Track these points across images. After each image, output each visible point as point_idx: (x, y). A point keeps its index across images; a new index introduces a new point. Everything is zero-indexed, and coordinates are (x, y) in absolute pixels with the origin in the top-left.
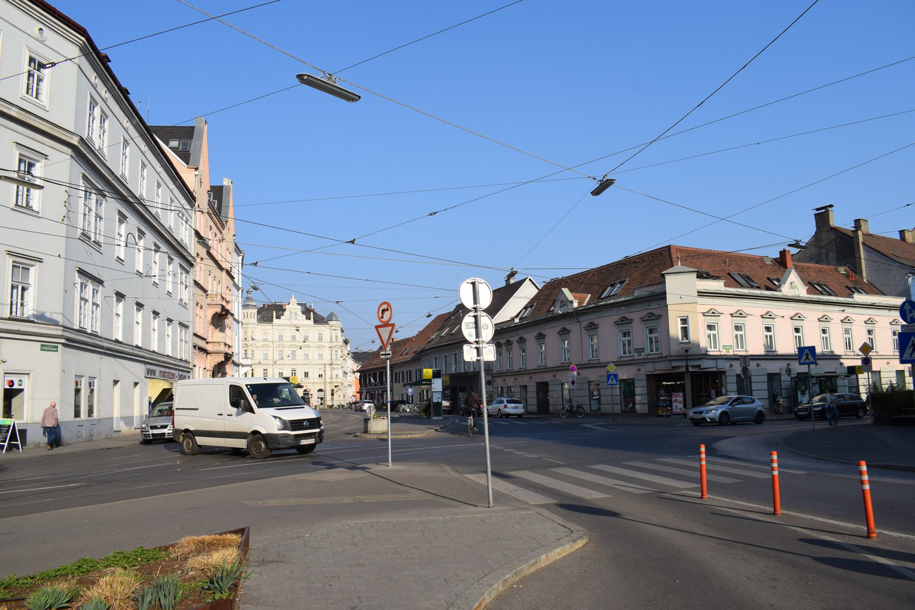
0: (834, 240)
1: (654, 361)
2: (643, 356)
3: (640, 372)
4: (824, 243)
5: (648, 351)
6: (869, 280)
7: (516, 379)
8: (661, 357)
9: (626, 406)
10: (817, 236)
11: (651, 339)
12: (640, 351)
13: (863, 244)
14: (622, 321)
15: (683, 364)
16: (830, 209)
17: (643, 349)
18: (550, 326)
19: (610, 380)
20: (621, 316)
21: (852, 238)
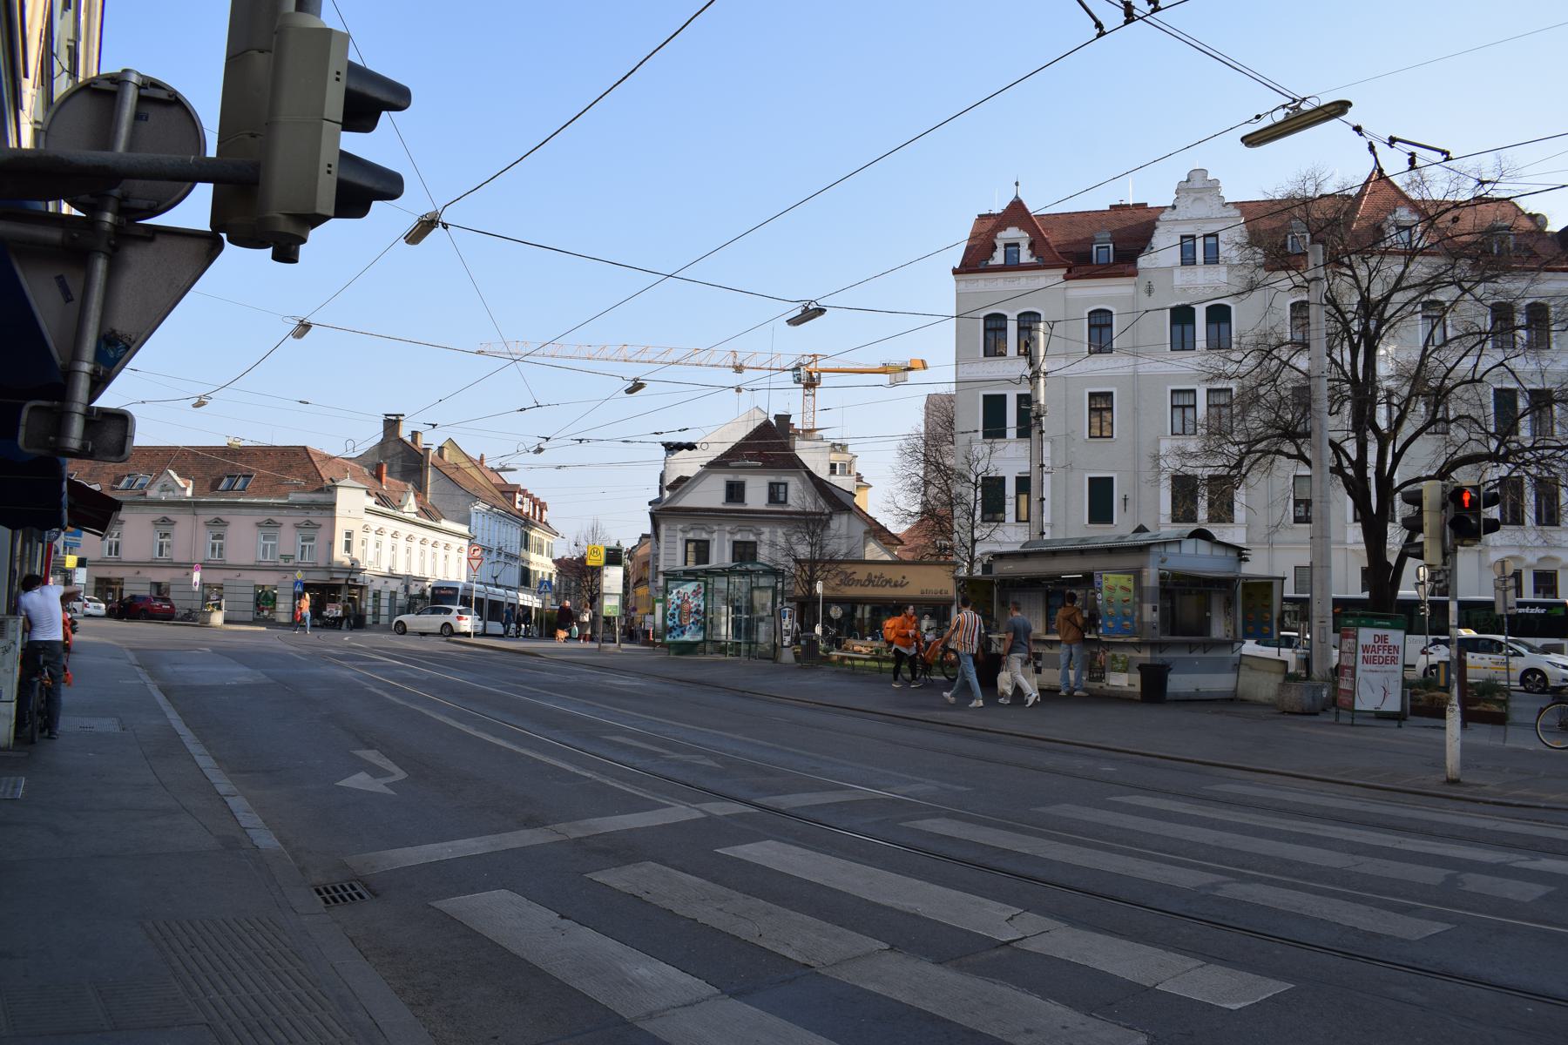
0: (401, 453)
1: (306, 570)
2: (291, 563)
3: (286, 580)
4: (390, 453)
5: (298, 558)
6: (432, 501)
7: (386, 582)
8: (317, 567)
9: (258, 614)
10: (382, 444)
11: (266, 545)
12: (286, 558)
13: (432, 463)
14: (269, 523)
15: (345, 576)
16: (401, 418)
17: (293, 556)
18: (135, 511)
19: (543, 587)
20: (268, 518)
21: (422, 456)
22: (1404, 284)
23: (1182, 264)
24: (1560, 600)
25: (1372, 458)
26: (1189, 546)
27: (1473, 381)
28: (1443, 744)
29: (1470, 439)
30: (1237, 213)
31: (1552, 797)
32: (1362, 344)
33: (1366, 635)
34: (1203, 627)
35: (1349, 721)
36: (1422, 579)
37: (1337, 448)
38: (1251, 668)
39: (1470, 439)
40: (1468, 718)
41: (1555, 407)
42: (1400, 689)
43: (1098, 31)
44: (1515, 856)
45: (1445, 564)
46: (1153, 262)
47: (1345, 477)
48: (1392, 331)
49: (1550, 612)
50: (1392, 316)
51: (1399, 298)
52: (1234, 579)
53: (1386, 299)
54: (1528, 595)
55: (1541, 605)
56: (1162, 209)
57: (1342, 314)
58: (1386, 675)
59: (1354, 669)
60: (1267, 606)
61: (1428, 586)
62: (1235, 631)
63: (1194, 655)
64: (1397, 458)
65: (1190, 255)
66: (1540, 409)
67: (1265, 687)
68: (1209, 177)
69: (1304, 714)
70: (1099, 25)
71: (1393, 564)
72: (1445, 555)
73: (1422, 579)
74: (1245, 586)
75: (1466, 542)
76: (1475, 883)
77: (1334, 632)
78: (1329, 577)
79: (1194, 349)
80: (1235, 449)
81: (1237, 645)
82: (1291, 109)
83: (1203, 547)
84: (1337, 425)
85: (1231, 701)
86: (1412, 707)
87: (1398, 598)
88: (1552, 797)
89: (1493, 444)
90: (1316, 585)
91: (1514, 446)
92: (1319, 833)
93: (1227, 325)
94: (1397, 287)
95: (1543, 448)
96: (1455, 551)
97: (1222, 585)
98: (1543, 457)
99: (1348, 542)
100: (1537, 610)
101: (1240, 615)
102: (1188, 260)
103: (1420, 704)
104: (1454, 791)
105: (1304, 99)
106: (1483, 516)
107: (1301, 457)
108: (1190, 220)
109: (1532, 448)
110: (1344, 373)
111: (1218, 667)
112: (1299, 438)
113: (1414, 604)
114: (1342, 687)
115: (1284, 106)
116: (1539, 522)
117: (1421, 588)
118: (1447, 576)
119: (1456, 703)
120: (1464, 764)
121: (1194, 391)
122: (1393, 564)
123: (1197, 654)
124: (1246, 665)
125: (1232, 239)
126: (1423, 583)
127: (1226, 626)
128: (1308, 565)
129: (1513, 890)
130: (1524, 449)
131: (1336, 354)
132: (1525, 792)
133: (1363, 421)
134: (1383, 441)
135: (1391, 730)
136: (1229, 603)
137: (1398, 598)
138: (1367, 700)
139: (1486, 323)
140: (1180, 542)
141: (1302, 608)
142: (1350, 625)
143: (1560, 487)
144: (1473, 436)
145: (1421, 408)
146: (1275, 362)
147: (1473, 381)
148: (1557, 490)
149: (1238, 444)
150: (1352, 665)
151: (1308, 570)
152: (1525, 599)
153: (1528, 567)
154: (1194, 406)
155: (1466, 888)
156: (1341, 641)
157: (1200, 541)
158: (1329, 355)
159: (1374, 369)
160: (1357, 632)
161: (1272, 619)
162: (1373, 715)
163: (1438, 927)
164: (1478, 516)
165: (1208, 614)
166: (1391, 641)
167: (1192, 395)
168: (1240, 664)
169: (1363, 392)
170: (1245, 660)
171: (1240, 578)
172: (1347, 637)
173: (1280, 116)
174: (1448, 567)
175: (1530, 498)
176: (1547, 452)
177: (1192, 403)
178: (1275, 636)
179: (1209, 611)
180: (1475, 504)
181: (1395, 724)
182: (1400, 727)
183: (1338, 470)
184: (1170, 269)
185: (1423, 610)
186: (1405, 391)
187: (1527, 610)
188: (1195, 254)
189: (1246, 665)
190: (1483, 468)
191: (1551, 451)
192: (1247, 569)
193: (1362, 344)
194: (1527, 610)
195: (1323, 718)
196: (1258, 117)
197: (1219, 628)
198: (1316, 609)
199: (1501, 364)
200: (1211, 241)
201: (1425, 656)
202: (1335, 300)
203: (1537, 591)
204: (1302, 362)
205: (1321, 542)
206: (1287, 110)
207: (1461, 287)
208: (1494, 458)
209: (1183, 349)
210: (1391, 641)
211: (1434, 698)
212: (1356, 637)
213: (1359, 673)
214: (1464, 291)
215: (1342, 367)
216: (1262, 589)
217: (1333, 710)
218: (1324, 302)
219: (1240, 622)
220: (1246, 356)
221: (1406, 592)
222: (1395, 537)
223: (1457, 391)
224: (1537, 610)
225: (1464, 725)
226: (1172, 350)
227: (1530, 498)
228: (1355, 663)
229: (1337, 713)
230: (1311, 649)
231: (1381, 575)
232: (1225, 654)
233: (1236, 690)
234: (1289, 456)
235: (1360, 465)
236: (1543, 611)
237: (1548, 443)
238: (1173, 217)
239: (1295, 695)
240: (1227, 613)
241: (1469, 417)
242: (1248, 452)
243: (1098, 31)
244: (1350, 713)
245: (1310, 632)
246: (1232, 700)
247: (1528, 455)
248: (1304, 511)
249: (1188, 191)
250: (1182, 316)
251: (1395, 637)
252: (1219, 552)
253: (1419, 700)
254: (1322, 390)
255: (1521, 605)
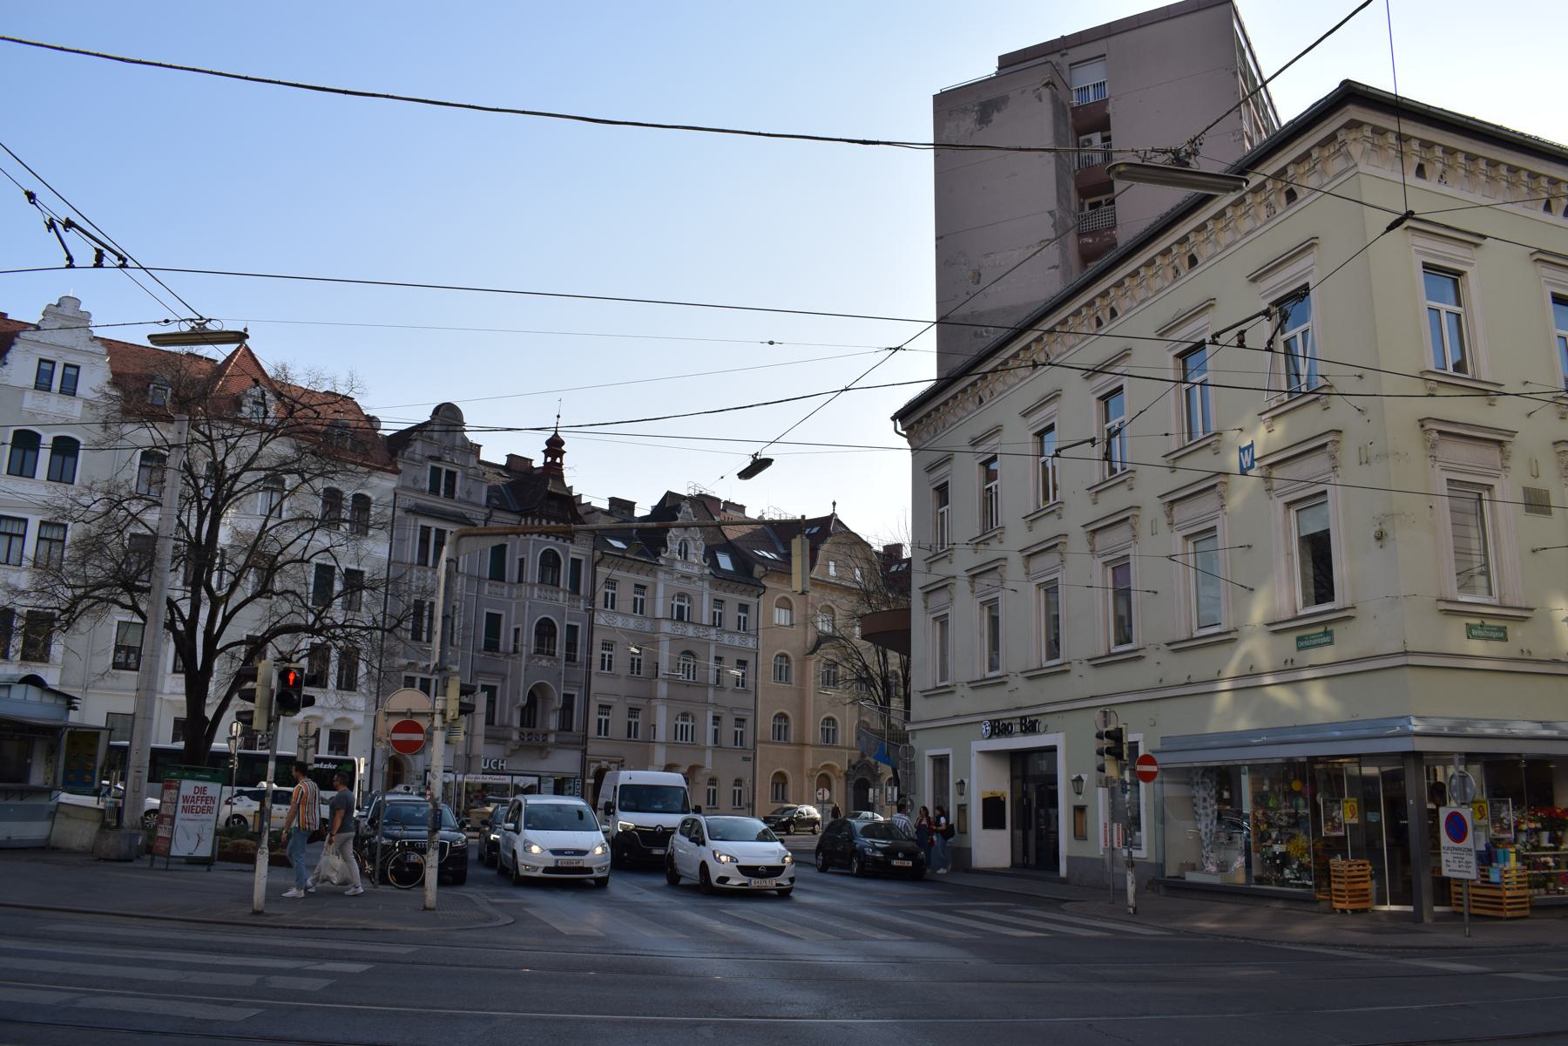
22: (254, 466)
23: (36, 388)
24: (349, 757)
25: (204, 613)
26: (18, 692)
27: (302, 561)
28: (251, 885)
29: (292, 612)
30: (104, 350)
31: (334, 920)
32: (209, 513)
33: (188, 787)
34: (23, 773)
35: (164, 866)
36: (234, 734)
37: (171, 604)
38: (68, 816)
39: (292, 612)
40: (274, 862)
41: (365, 593)
42: (212, 836)
43: (68, 263)
44: (307, 963)
45: (268, 730)
46: (4, 378)
47: (176, 633)
48: (237, 503)
49: (340, 768)
50: (241, 490)
51: (248, 477)
52: (60, 728)
53: (236, 477)
54: (324, 753)
55: (333, 761)
56: (25, 326)
57: (195, 478)
58: (200, 823)
59: (173, 818)
60: (92, 755)
61: (239, 740)
62: (55, 778)
63: (10, 802)
64: (226, 620)
65: (46, 380)
66: (352, 593)
67: (81, 834)
68: (82, 308)
69: (119, 861)
70: (70, 258)
71: (210, 719)
72: (269, 722)
73: (234, 734)
74: (70, 734)
75: (288, 713)
76: (278, 982)
77: (150, 780)
78: (150, 729)
79: (33, 477)
80: (69, 593)
81: (55, 793)
82: (197, 324)
83: (33, 693)
84: (174, 584)
85: (45, 849)
86: (219, 853)
87: (212, 750)
88: (334, 920)
89: (311, 618)
90: (136, 736)
91: (328, 621)
92: (152, 957)
93: (73, 460)
94: (247, 467)
95: (351, 626)
96: (278, 719)
97: (48, 733)
98: (350, 634)
99: (165, 691)
100: (330, 766)
101: (62, 763)
102: (43, 383)
103: (226, 850)
104: (259, 920)
105: (210, 320)
106: (304, 693)
107: (135, 608)
108: (52, 345)
109: (343, 627)
110: (189, 535)
111: (33, 815)
112: (136, 592)
113: (226, 756)
114: (160, 834)
115: (191, 320)
116: (339, 687)
117: (232, 742)
118: (269, 740)
119: (266, 846)
120: (268, 899)
121: (26, 521)
122: (210, 719)
123: (13, 802)
124: (63, 813)
125: (95, 378)
126: (235, 738)
127: (46, 773)
128: (132, 712)
129: (307, 984)
130: (336, 626)
131: (184, 518)
132: (315, 918)
133: (197, 582)
134: (215, 602)
135: (200, 872)
136: (52, 751)
137: (212, 750)
138: (182, 847)
139: (317, 509)
140: (9, 687)
141: (119, 758)
142: (173, 777)
143: (361, 661)
144: (296, 609)
145: (252, 577)
146: (123, 513)
147: (302, 561)
148: (357, 663)
149: (74, 587)
150: (171, 813)
151: (130, 718)
152: (320, 755)
153: (326, 726)
154: (23, 536)
155: (273, 986)
156: (163, 791)
157: (30, 687)
158: (178, 517)
159: (216, 536)
160: (180, 784)
161: (95, 767)
162: (183, 860)
163: (254, 1012)
164: (299, 692)
165: (29, 761)
166: (209, 793)
167: (23, 525)
168: (56, 812)
169: (200, 556)
170: (62, 808)
171: (67, 727)
172: (169, 787)
173: (186, 328)
174: (271, 733)
175: (333, 668)
176: (354, 630)
177: (21, 532)
178: (96, 785)
179: (31, 758)
180: (298, 683)
181: (205, 868)
182: (209, 870)
183: (170, 625)
184: (23, 390)
185: (233, 763)
186: (241, 560)
187: (321, 766)
188: (51, 381)
189: (63, 813)
190: (300, 638)
191: (357, 630)
192: (74, 717)
193: (209, 513)
194: (321, 766)
195: (136, 864)
196: (167, 321)
197: (38, 776)
198: (133, 758)
199: (327, 550)
200: (72, 372)
201: (229, 806)
202: (191, 467)
203: (331, 748)
204: (152, 517)
205: (147, 692)
206: (193, 324)
207: (303, 478)
208: (310, 629)
209: (21, 475)
210: (209, 793)
211: (238, 845)
212: (178, 789)
213: (177, 821)
214: (305, 481)
215: (187, 529)
216: (84, 738)
217: (148, 857)
218: (182, 468)
219: (61, 770)
220: (95, 502)
221: (219, 745)
222: (215, 690)
223: (287, 567)
224: (330, 766)
225: (271, 863)
226: (8, 473)
227: (333, 668)
228: (175, 812)
229: (152, 859)
230: (123, 797)
231: (195, 727)
232: (42, 801)
233: (49, 837)
234: (124, 606)
235: (192, 623)
236: (334, 767)
237: (356, 623)
238: (35, 338)
239: (112, 842)
240: (48, 761)
241: (293, 592)
242: (86, 596)
243: (68, 263)
244: (165, 859)
245: (123, 778)
246: (43, 848)
247: (339, 631)
248: (128, 657)
249: (57, 316)
250: (26, 441)
251: (213, 789)
252: (49, 699)
253: (226, 846)
254: (166, 550)
255: (318, 761)
